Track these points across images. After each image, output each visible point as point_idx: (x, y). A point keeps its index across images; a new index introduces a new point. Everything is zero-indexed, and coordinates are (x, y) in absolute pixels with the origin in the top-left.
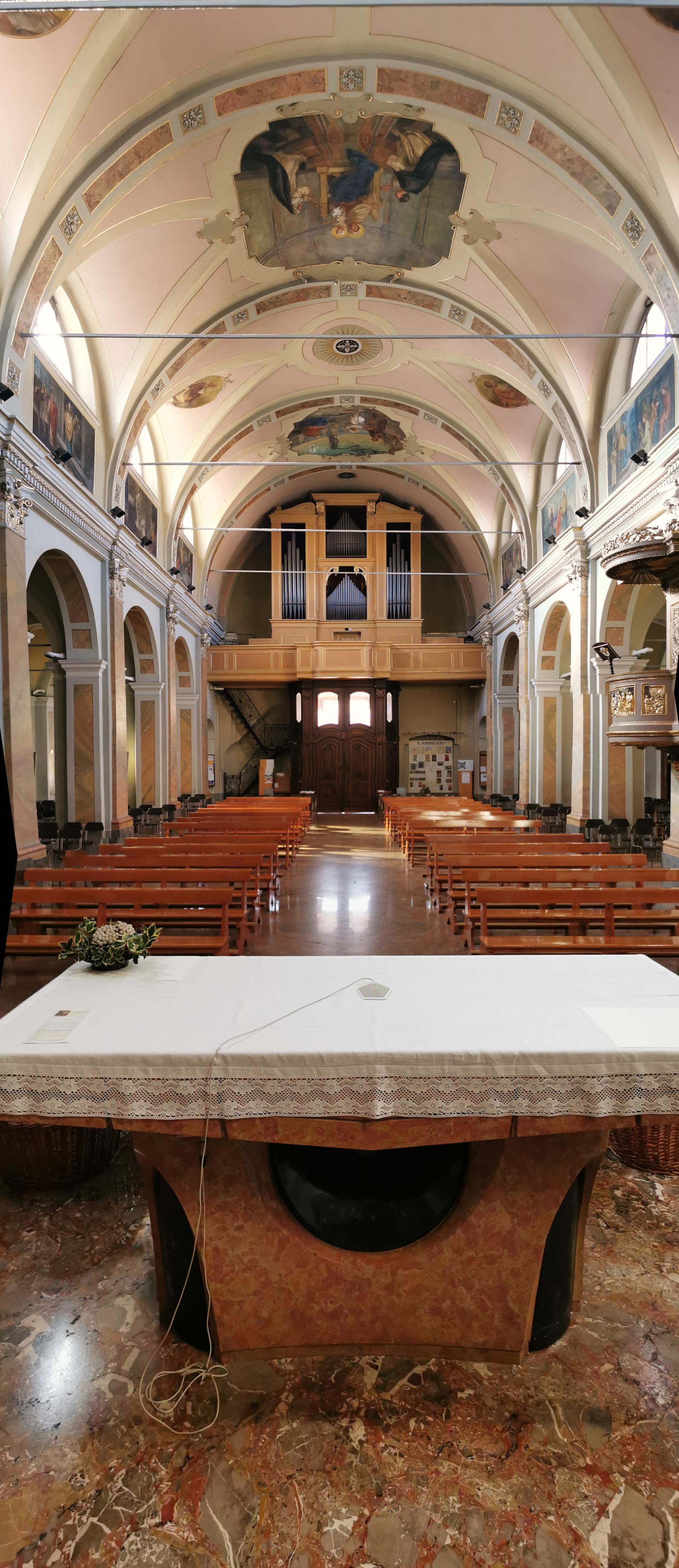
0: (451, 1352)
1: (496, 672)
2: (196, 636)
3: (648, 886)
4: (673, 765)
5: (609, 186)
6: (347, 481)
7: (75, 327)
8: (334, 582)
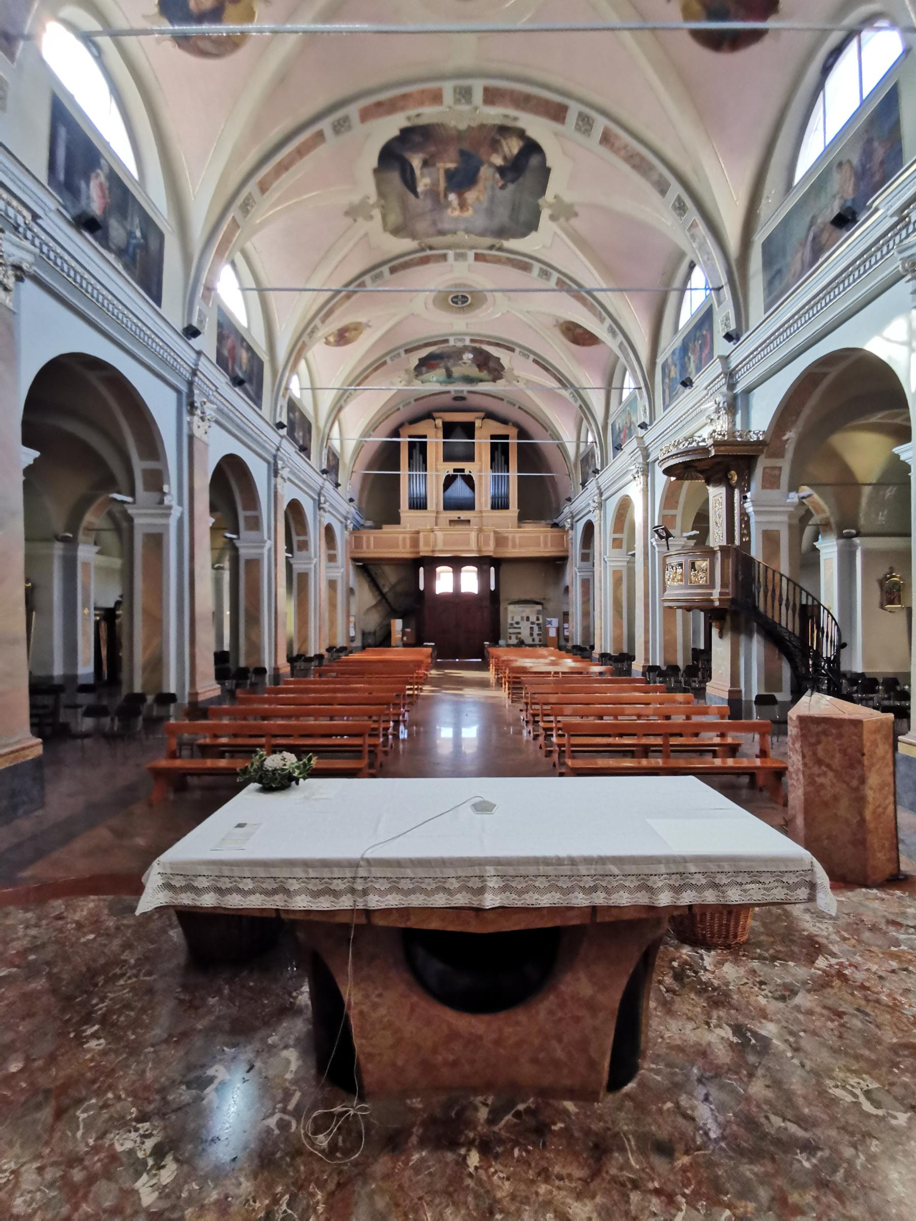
0: (547, 1093)
1: (576, 551)
2: (341, 522)
3: (696, 719)
4: (714, 624)
5: (661, 176)
6: (459, 403)
7: (250, 283)
8: (449, 481)
